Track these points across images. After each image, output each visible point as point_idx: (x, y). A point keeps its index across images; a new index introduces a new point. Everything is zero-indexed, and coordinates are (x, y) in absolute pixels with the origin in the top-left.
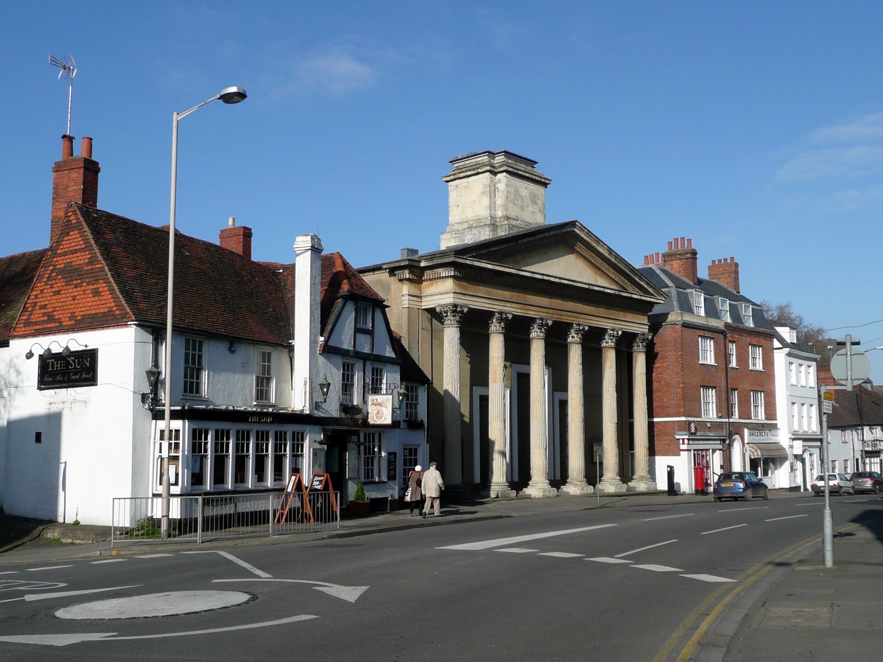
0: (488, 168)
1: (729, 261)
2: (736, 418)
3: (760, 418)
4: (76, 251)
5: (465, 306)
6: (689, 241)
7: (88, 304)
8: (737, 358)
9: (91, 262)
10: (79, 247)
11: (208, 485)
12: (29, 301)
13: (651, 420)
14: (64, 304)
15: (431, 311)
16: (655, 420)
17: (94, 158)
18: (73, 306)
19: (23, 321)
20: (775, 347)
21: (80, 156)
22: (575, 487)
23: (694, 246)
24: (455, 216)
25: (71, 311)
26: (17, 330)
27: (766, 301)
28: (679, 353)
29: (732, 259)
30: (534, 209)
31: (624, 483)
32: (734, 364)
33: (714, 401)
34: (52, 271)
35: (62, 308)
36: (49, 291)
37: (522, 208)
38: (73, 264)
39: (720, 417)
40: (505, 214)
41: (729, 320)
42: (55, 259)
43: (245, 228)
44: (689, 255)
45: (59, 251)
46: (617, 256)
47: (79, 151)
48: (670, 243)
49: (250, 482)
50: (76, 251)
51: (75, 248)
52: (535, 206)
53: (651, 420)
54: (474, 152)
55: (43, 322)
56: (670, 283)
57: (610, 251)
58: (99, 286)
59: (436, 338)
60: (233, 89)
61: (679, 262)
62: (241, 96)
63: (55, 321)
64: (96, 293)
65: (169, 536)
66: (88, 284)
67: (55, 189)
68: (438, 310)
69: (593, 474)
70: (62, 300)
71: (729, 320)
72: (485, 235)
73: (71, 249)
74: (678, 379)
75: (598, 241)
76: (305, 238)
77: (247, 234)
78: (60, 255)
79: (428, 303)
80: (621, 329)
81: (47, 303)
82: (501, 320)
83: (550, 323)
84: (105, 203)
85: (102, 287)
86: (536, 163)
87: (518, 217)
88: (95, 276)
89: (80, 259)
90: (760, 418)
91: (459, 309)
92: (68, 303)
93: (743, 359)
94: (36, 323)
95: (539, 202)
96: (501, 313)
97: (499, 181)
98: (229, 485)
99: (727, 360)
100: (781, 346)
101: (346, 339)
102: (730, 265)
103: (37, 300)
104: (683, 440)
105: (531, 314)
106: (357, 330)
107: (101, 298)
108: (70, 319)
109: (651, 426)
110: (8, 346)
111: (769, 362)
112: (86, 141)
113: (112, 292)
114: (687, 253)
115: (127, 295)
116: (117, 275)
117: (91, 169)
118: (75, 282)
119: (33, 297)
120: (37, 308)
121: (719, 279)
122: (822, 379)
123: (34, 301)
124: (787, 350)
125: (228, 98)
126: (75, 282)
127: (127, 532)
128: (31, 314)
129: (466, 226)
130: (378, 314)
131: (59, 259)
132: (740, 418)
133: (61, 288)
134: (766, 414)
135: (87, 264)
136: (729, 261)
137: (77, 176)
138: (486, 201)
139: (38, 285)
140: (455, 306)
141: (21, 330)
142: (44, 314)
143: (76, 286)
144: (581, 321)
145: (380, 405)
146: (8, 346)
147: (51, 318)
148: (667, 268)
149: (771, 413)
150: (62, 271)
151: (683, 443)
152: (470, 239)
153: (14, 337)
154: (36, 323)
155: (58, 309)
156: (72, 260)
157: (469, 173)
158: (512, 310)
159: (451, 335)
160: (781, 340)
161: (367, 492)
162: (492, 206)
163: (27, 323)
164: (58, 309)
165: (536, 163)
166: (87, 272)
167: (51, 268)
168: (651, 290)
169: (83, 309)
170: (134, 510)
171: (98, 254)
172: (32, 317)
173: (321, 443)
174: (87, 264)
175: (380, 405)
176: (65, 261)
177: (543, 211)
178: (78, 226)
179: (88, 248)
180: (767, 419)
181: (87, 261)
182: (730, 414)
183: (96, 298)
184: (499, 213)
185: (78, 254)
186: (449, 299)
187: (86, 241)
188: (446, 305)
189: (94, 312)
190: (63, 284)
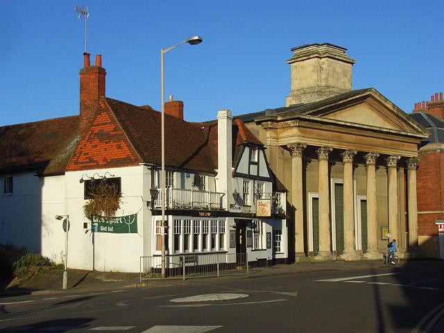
0: (317, 55)
4: (106, 124)
5: (305, 144)
7: (115, 153)
9: (115, 130)
11: (181, 251)
15: (285, 147)
17: (103, 67)
21: (95, 65)
24: (295, 85)
30: (344, 80)
34: (91, 134)
36: (89, 145)
37: (338, 79)
43: (180, 102)
46: (398, 109)
47: (93, 63)
49: (208, 249)
50: (106, 124)
52: (346, 78)
54: (306, 44)
55: (87, 162)
57: (394, 106)
59: (288, 162)
60: (196, 38)
61: (438, 109)
62: (199, 41)
63: (94, 162)
64: (119, 147)
65: (166, 277)
66: (114, 142)
67: (81, 84)
68: (288, 146)
72: (316, 99)
75: (386, 100)
76: (223, 112)
77: (181, 105)
78: (96, 126)
79: (283, 142)
80: (400, 155)
82: (325, 151)
83: (356, 153)
84: (111, 93)
85: (123, 144)
88: (118, 138)
89: (109, 128)
91: (301, 146)
94: (82, 163)
95: (348, 75)
96: (325, 147)
97: (323, 63)
98: (190, 250)
101: (243, 168)
104: (441, 225)
105: (344, 147)
106: (251, 163)
108: (103, 161)
112: (99, 57)
113: (129, 146)
115: (137, 148)
116: (131, 138)
117: (102, 72)
125: (193, 42)
127: (144, 275)
128: (79, 157)
130: (261, 152)
137: (94, 77)
140: (299, 144)
141: (73, 166)
142: (87, 158)
143: (107, 143)
144: (375, 151)
145: (264, 205)
147: (91, 161)
148: (430, 112)
150: (97, 134)
152: (305, 100)
153: (67, 170)
154: (82, 163)
157: (304, 58)
158: (333, 145)
159: (297, 161)
161: (12, 278)
162: (319, 79)
163: (76, 163)
168: (419, 130)
170: (145, 263)
171: (120, 126)
173: (234, 227)
174: (113, 131)
175: (264, 205)
177: (351, 81)
178: (107, 111)
179: (113, 122)
186: (295, 140)
187: (111, 118)
188: (294, 144)
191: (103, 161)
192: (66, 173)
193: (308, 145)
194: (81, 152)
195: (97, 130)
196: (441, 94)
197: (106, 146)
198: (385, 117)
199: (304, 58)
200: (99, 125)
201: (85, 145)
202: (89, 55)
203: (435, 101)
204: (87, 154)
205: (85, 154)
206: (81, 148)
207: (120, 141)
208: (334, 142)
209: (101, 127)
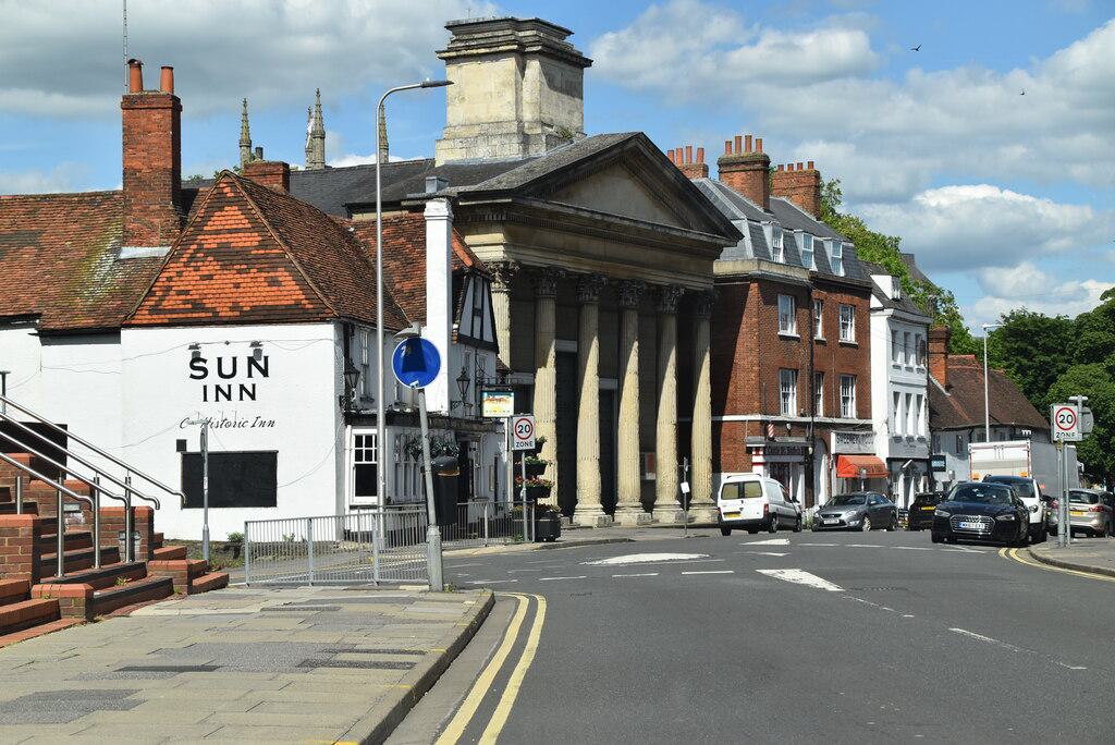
1: (805, 167)
2: (821, 417)
3: (849, 416)
4: (237, 231)
6: (759, 142)
7: (256, 291)
8: (824, 326)
9: (262, 245)
10: (241, 226)
12: (157, 284)
13: (718, 419)
14: (220, 291)
16: (725, 418)
17: (175, 94)
18: (237, 295)
19: (148, 308)
20: (872, 306)
22: (628, 516)
23: (765, 151)
24: (456, 114)
25: (234, 300)
26: (136, 317)
27: (1008, 315)
28: (755, 320)
29: (811, 164)
31: (646, 511)
32: (819, 335)
33: (854, 396)
34: (196, 251)
35: (217, 296)
36: (191, 276)
38: (232, 245)
39: (802, 415)
40: (537, 116)
41: (814, 268)
42: (199, 237)
44: (758, 166)
45: (205, 228)
48: (729, 143)
50: (237, 231)
51: (235, 226)
53: (718, 419)
56: (738, 213)
58: (277, 274)
64: (273, 282)
69: (609, 499)
70: (216, 286)
71: (814, 268)
73: (226, 227)
74: (750, 359)
78: (209, 233)
80: (683, 286)
81: (190, 288)
85: (282, 274)
86: (570, 33)
87: (552, 120)
88: (272, 264)
89: (250, 240)
90: (849, 416)
92: (227, 291)
93: (832, 330)
99: (813, 331)
100: (881, 305)
102: (808, 175)
103: (172, 284)
107: (281, 288)
108: (232, 309)
109: (717, 427)
110: (118, 341)
111: (864, 332)
114: (756, 162)
118: (238, 267)
119: (164, 279)
120: (172, 293)
121: (789, 196)
122: (595, 258)
123: (167, 284)
124: (889, 312)
126: (238, 267)
129: (477, 130)
131: (207, 237)
132: (826, 415)
133: (214, 272)
134: (858, 410)
135: (257, 248)
136: (805, 167)
138: (510, 96)
139: (172, 265)
142: (185, 302)
143: (239, 272)
146: (118, 341)
149: (864, 409)
150: (209, 252)
151: (757, 455)
155: (209, 296)
156: (230, 240)
160: (881, 296)
163: (155, 310)
164: (209, 296)
165: (570, 33)
166: (257, 257)
167: (195, 247)
169: (252, 299)
172: (165, 303)
174: (257, 248)
176: (219, 241)
179: (256, 226)
180: (859, 417)
181: (256, 244)
182: (813, 413)
183: (274, 288)
184: (528, 115)
185: (240, 235)
189: (270, 303)
190: (218, 267)
191: (232, 309)
192: (125, 333)
193: (687, 291)
194: (169, 288)
195: (211, 242)
196: (437, 52)
197: (238, 278)
198: (657, 198)
199: (483, 51)
200: (217, 232)
201: (180, 274)
202: (172, 69)
203: (734, 154)
204: (187, 292)
205: (179, 293)
206: (169, 279)
207: (274, 268)
208: (566, 258)
209: (222, 238)
